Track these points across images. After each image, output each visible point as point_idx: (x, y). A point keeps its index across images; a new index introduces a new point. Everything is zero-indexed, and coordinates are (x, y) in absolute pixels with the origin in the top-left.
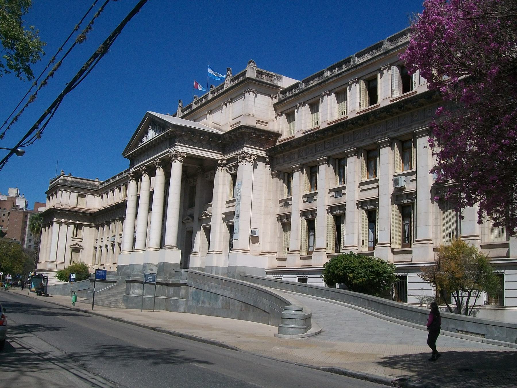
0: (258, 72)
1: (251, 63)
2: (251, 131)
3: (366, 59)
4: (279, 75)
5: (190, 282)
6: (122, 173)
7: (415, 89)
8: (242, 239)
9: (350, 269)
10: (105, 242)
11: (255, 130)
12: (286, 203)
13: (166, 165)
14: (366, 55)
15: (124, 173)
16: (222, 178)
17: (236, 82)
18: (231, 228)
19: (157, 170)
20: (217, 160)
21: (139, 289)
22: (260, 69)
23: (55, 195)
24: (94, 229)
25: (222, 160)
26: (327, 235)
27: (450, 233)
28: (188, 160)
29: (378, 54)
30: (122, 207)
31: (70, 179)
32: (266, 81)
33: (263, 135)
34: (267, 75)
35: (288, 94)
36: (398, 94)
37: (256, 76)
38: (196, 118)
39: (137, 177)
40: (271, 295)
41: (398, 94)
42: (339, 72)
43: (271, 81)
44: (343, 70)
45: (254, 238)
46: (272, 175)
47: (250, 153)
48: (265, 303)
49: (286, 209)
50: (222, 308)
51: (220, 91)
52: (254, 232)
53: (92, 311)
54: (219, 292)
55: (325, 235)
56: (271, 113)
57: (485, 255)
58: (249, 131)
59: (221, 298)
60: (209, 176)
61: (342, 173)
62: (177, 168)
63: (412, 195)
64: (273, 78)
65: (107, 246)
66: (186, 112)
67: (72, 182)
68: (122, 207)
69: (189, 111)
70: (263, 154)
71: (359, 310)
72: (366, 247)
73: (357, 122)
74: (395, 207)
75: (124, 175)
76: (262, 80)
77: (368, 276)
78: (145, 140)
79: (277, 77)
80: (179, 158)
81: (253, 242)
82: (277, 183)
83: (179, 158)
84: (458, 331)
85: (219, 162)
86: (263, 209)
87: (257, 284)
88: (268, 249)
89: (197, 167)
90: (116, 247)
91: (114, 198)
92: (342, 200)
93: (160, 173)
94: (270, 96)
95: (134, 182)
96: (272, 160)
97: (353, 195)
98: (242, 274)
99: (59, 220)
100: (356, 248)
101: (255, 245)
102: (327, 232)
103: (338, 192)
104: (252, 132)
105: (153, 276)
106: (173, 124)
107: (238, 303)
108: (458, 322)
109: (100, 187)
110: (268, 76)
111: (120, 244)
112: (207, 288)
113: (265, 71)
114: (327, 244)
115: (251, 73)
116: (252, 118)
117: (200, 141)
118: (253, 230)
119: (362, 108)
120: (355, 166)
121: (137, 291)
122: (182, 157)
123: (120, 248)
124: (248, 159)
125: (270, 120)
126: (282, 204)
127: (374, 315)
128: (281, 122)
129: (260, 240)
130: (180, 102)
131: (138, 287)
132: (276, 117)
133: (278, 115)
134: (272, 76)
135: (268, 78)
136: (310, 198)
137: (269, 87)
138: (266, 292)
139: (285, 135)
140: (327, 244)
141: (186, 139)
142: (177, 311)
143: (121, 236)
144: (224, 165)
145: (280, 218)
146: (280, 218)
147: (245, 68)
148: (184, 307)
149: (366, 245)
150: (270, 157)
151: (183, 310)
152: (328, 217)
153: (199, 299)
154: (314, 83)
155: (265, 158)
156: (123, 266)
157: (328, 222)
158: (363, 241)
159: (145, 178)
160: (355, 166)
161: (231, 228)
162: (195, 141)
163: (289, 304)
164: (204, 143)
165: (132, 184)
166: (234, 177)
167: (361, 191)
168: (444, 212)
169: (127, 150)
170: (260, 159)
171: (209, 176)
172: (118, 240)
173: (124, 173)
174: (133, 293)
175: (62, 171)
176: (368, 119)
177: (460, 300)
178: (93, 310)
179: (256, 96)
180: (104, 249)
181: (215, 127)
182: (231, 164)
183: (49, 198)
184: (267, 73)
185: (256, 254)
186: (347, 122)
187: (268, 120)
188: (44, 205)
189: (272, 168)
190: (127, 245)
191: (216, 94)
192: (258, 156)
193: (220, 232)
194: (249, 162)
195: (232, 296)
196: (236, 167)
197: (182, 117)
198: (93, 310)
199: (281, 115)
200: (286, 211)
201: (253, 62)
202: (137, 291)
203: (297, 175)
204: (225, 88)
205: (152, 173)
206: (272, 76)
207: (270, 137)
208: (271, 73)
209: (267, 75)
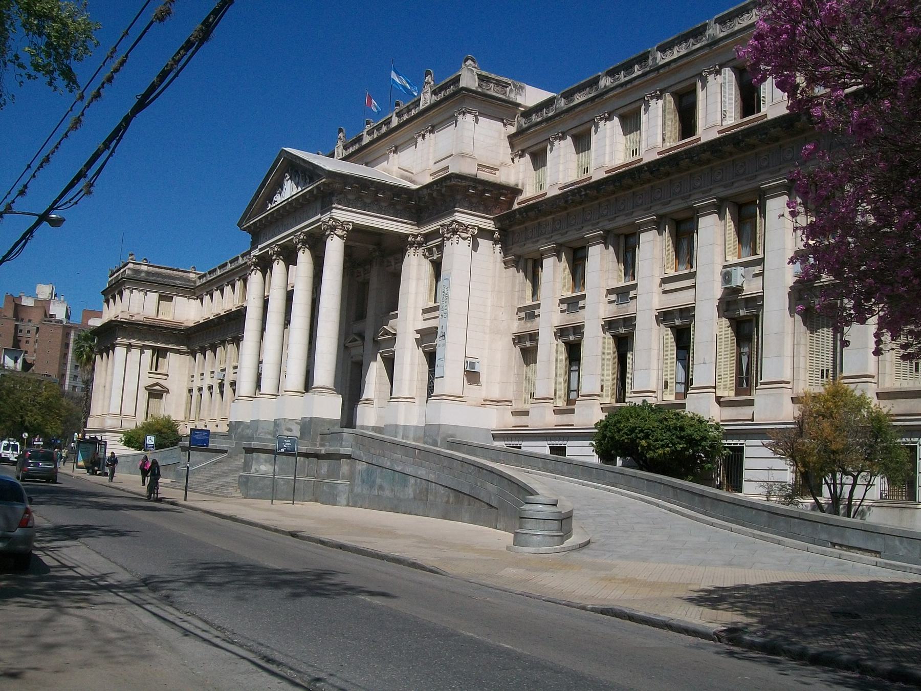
0: (482, 78)
1: (469, 62)
3: (676, 56)
5: (358, 452)
6: (237, 259)
7: (763, 110)
8: (451, 376)
10: (208, 381)
12: (530, 313)
13: (316, 243)
14: (676, 48)
15: (240, 259)
16: (415, 268)
17: (441, 96)
18: (431, 357)
19: (300, 253)
20: (407, 236)
21: (268, 465)
22: (484, 73)
23: (118, 297)
25: (416, 236)
26: (603, 371)
27: (822, 371)
29: (698, 46)
30: (236, 318)
31: (144, 268)
32: (495, 94)
34: (498, 83)
35: (535, 118)
36: (732, 119)
37: (477, 85)
38: (368, 160)
39: (265, 265)
40: (501, 475)
41: (732, 119)
42: (626, 79)
43: (505, 94)
44: (634, 75)
45: (472, 376)
47: (466, 223)
48: (491, 489)
49: (529, 325)
51: (413, 112)
52: (473, 365)
53: (184, 503)
54: (408, 470)
55: (599, 372)
56: (505, 150)
57: (885, 411)
58: (464, 183)
59: (412, 480)
62: (334, 249)
63: (756, 302)
64: (508, 89)
65: (210, 388)
66: (351, 150)
67: (147, 273)
68: (236, 318)
69: (356, 147)
70: (489, 225)
71: (658, 505)
72: (671, 393)
74: (725, 322)
75: (241, 261)
76: (489, 92)
77: (674, 445)
78: (278, 199)
79: (515, 86)
80: (339, 232)
82: (514, 276)
83: (339, 232)
84: (834, 545)
85: (410, 239)
86: (488, 323)
88: (496, 395)
89: (371, 247)
90: (227, 389)
92: (629, 309)
93: (304, 258)
94: (502, 120)
95: (259, 274)
97: (650, 300)
98: (449, 439)
99: (127, 341)
100: (653, 395)
102: (603, 366)
103: (622, 294)
104: (470, 186)
105: (293, 442)
106: (329, 171)
107: (442, 490)
111: (233, 384)
112: (388, 464)
113: (493, 76)
114: (602, 386)
115: (469, 79)
118: (469, 360)
119: (669, 145)
120: (654, 248)
121: (263, 468)
122: (344, 230)
123: (234, 391)
124: (462, 234)
126: (523, 315)
128: (522, 168)
129: (483, 378)
130: (340, 131)
131: (266, 461)
132: (513, 160)
133: (516, 156)
135: (499, 88)
136: (572, 304)
138: (492, 471)
139: (529, 192)
140: (602, 386)
141: (351, 197)
142: (334, 503)
143: (235, 371)
144: (420, 245)
145: (518, 339)
146: (518, 339)
150: (501, 230)
151: (345, 503)
152: (604, 338)
155: (493, 232)
156: (239, 423)
157: (604, 348)
158: (666, 383)
159: (278, 267)
160: (654, 248)
161: (431, 357)
162: (368, 201)
163: (532, 492)
164: (383, 204)
165: (255, 278)
166: (437, 266)
167: (665, 292)
168: (812, 332)
169: (246, 217)
170: (484, 233)
172: (229, 377)
173: (240, 259)
175: (132, 255)
177: (838, 490)
179: (477, 121)
180: (205, 392)
181: (406, 178)
183: (107, 301)
184: (497, 80)
185: (474, 403)
186: (640, 169)
187: (498, 164)
188: (99, 315)
189: (505, 251)
190: (246, 386)
191: (405, 117)
192: (480, 229)
193: (412, 364)
194: (464, 239)
195: (432, 477)
196: (440, 248)
197: (344, 159)
200: (529, 327)
201: (472, 60)
202: (263, 468)
203: (549, 263)
204: (422, 107)
205: (290, 258)
207: (502, 194)
208: (505, 79)
209: (498, 83)
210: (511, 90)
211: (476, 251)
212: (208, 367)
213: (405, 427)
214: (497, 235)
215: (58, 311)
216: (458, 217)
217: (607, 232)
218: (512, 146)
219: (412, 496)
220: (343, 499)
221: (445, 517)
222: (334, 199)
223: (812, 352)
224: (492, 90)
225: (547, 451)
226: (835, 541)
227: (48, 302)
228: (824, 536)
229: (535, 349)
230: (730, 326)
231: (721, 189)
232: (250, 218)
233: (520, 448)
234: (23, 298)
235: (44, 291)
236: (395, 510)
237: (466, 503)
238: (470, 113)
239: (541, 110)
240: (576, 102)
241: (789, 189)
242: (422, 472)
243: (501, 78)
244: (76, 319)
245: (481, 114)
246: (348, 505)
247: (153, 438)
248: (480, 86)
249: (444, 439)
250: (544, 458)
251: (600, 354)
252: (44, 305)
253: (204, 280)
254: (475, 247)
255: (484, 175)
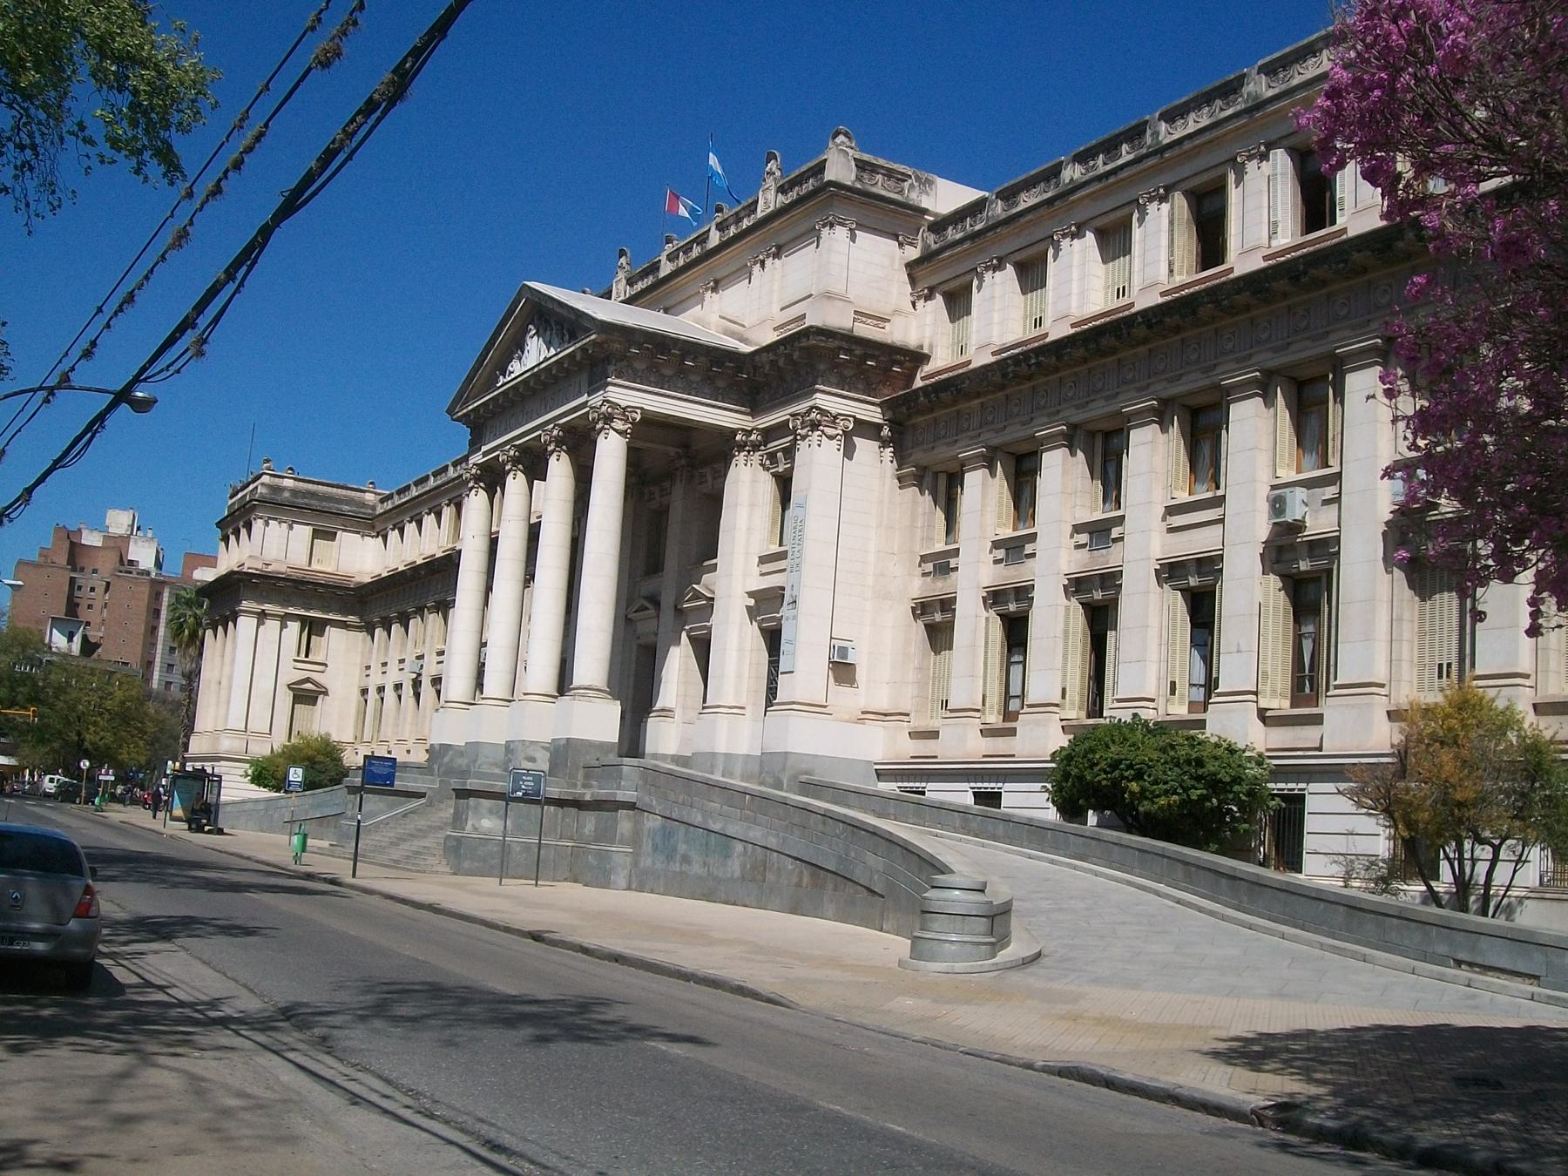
0: (862, 166)
1: (841, 138)
2: (837, 343)
3: (1191, 129)
4: (924, 175)
5: (647, 799)
7: (1341, 221)
9: (1130, 767)
10: (394, 675)
11: (848, 340)
12: (941, 564)
14: (1192, 116)
15: (451, 469)
16: (746, 485)
17: (793, 195)
18: (773, 639)
19: (553, 460)
20: (734, 432)
22: (866, 157)
23: (243, 532)
24: (361, 636)
25: (748, 433)
27: (1440, 666)
28: (650, 435)
29: (1230, 111)
30: (443, 570)
31: (288, 483)
32: (884, 193)
33: (872, 358)
34: (890, 174)
35: (952, 234)
37: (853, 177)
39: (492, 479)
42: (1108, 168)
43: (901, 192)
44: (1120, 162)
45: (843, 670)
46: (899, 479)
47: (834, 411)
49: (939, 584)
50: (743, 878)
51: (746, 223)
55: (1060, 665)
56: (900, 289)
58: (832, 344)
59: (739, 847)
60: (709, 479)
61: (1112, 476)
62: (610, 453)
63: (1327, 548)
64: (906, 185)
65: (398, 687)
66: (640, 286)
67: (294, 492)
68: (443, 570)
69: (649, 281)
70: (873, 414)
71: (1157, 893)
73: (1160, 322)
74: (1274, 581)
77: (1186, 790)
78: (516, 368)
79: (918, 179)
80: (619, 425)
81: (839, 680)
82: (915, 502)
84: (1459, 963)
85: (738, 437)
86: (870, 581)
87: (849, 807)
88: (883, 704)
89: (672, 451)
90: (427, 689)
91: (418, 544)
92: (1110, 558)
93: (560, 468)
94: (895, 237)
95: (483, 494)
96: (902, 433)
97: (1145, 543)
98: (803, 778)
99: (257, 607)
101: (845, 690)
104: (840, 348)
105: (537, 779)
107: (789, 864)
108: (1460, 937)
109: (379, 510)
110: (890, 177)
111: (437, 681)
112: (698, 819)
113: (881, 162)
114: (1064, 690)
115: (840, 167)
116: (841, 304)
117: (682, 372)
118: (838, 643)
119: (1179, 279)
120: (1153, 455)
121: (486, 823)
122: (626, 421)
123: (438, 692)
125: (896, 312)
126: (929, 567)
127: (1200, 909)
128: (929, 319)
129: (861, 675)
130: (622, 253)
131: (490, 812)
132: (914, 304)
133: (919, 298)
134: (904, 177)
135: (892, 183)
136: (1014, 549)
137: (891, 210)
139: (942, 359)
140: (1064, 690)
142: (604, 883)
144: (756, 447)
146: (921, 609)
147: (822, 152)
148: (626, 872)
149: (1182, 696)
150: (893, 423)
151: (623, 883)
152: (1067, 608)
153: (675, 849)
154: (1032, 201)
155: (879, 427)
157: (1067, 624)
159: (515, 483)
160: (1153, 455)
161: (773, 639)
162: (668, 372)
163: (943, 869)
165: (476, 502)
166: (784, 484)
167: (1171, 530)
168: (1423, 600)
170: (865, 429)
171: (709, 479)
173: (451, 469)
174: (475, 829)
176: (1194, 312)
177: (1468, 870)
178: (354, 875)
179: (853, 238)
180: (390, 694)
181: (727, 333)
182: (774, 445)
183: (226, 539)
184: (888, 169)
188: (211, 561)
189: (900, 458)
190: (458, 684)
191: (733, 231)
193: (741, 650)
194: (831, 438)
195: (772, 842)
196: (790, 452)
197: (627, 301)
198: (354, 875)
199: (928, 298)
200: (939, 587)
201: (846, 135)
202: (486, 823)
204: (760, 214)
206: (904, 177)
209: (890, 174)
210: (912, 186)
211: (850, 458)
212: (395, 651)
213: (728, 756)
214: (886, 432)
215: (143, 554)
216: (821, 400)
217: (1074, 427)
218: (913, 281)
219: (737, 874)
220: (621, 878)
221: (794, 911)
222: (611, 368)
223: (1422, 634)
224: (880, 186)
225: (969, 799)
226: (1461, 956)
227: (126, 539)
228: (1442, 949)
229: (949, 626)
230: (1283, 588)
231: (1270, 355)
232: (466, 402)
233: (923, 793)
234: (85, 533)
235: (119, 521)
236: (709, 897)
237: (830, 886)
238: (843, 225)
239: (962, 220)
240: (1022, 206)
241: (1384, 355)
242: (756, 834)
243: (895, 166)
244: (173, 569)
245: (861, 227)
246: (629, 889)
247: (300, 771)
248: (858, 179)
249: (795, 777)
250: (963, 811)
251: (1060, 633)
252: (118, 545)
253: (389, 505)
254: (849, 452)
255: (865, 330)
